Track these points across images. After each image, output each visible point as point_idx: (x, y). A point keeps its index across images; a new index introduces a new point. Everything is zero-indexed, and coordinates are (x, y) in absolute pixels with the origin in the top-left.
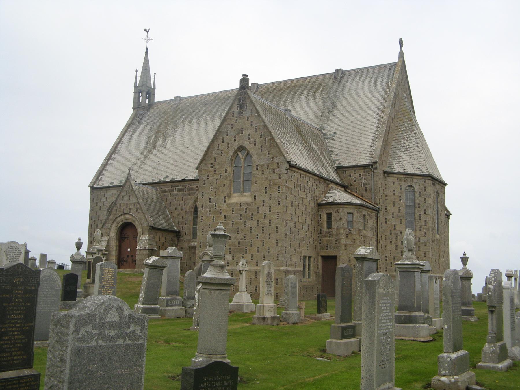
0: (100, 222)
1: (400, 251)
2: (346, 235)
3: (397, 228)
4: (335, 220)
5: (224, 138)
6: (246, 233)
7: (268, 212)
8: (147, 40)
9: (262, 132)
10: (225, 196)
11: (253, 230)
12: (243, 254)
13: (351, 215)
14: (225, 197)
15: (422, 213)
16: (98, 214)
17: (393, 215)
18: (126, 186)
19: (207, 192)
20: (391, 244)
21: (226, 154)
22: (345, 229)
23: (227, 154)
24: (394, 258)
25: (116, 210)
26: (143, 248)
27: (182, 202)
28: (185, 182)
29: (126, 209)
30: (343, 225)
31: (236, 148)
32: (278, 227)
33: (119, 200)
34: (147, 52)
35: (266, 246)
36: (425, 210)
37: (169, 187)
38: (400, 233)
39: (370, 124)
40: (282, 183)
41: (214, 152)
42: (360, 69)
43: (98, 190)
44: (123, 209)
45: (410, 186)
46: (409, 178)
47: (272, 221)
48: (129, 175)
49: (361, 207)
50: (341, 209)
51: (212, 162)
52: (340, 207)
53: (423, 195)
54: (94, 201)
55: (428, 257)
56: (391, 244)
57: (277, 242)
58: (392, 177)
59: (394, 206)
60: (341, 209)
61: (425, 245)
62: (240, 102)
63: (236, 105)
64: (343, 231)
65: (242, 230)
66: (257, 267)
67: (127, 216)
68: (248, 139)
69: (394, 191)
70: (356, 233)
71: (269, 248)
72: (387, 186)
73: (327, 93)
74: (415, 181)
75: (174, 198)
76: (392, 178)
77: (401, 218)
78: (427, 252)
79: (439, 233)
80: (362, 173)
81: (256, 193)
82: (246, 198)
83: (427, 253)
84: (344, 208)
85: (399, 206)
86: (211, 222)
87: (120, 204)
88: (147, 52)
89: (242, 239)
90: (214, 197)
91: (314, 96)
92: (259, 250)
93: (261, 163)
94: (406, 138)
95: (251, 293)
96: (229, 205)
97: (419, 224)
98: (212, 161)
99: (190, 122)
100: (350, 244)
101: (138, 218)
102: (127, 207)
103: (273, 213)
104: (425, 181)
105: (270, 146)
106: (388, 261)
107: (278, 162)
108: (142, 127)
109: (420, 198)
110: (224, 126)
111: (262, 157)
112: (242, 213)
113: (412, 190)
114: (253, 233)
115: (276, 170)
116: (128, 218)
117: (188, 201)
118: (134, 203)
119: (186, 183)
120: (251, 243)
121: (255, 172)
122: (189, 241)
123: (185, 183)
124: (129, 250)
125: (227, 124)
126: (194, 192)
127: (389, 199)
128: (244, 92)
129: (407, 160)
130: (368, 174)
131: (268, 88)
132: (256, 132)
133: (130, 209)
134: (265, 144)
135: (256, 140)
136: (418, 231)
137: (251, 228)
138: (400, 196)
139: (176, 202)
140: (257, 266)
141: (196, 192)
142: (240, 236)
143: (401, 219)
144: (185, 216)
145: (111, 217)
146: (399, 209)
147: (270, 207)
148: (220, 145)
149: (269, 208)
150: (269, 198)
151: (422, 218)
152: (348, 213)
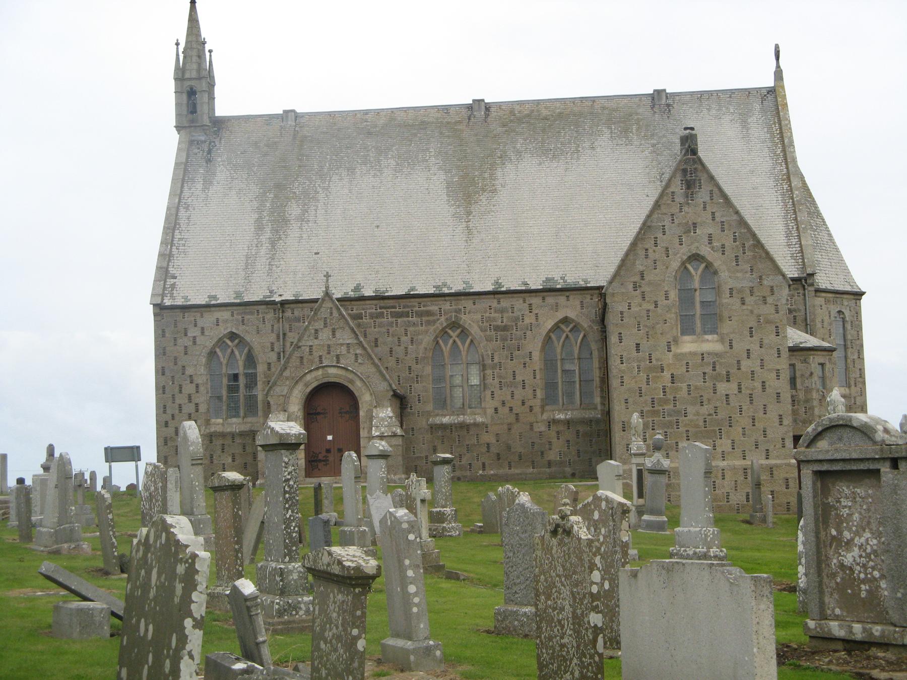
0: (188, 379)
4: (802, 375)
5: (657, 238)
6: (718, 404)
7: (759, 368)
9: (735, 233)
10: (670, 340)
11: (730, 399)
12: (714, 440)
14: (669, 342)
16: (180, 363)
18: (322, 310)
19: (629, 333)
21: (664, 267)
23: (667, 268)
25: (302, 358)
26: (390, 434)
27: (404, 339)
28: (412, 300)
29: (328, 356)
31: (685, 257)
32: (779, 394)
33: (306, 338)
35: (760, 425)
37: (371, 308)
39: (768, 202)
40: (781, 321)
41: (637, 262)
42: (702, 93)
43: (178, 310)
44: (320, 357)
47: (767, 384)
48: (327, 288)
50: (811, 357)
51: (635, 280)
52: (810, 355)
54: (167, 335)
57: (780, 419)
60: (811, 357)
62: (685, 175)
63: (678, 181)
65: (709, 400)
66: (745, 461)
67: (332, 371)
68: (709, 243)
71: (765, 428)
73: (653, 135)
75: (384, 330)
76: (819, 299)
81: (731, 336)
82: (711, 344)
84: (815, 356)
86: (644, 387)
87: (311, 346)
89: (710, 415)
90: (645, 342)
91: (627, 138)
92: (747, 433)
93: (739, 286)
95: (738, 504)
96: (678, 357)
98: (637, 278)
99: (351, 170)
101: (361, 374)
102: (329, 353)
103: (768, 370)
105: (754, 257)
107: (771, 284)
108: (222, 174)
110: (655, 216)
111: (739, 275)
112: (706, 371)
114: (732, 405)
115: (768, 299)
116: (334, 374)
117: (420, 337)
118: (348, 344)
119: (414, 302)
121: (726, 301)
122: (429, 414)
123: (410, 302)
124: (330, 438)
125: (662, 214)
126: (435, 318)
128: (693, 160)
130: (798, 293)
131: (512, 112)
132: (724, 231)
133: (338, 357)
134: (744, 253)
135: (724, 245)
136: (853, 387)
137: (727, 395)
139: (390, 339)
140: (744, 459)
141: (438, 320)
142: (705, 409)
144: (414, 367)
145: (287, 373)
147: (762, 360)
148: (650, 251)
149: (759, 361)
150: (759, 345)
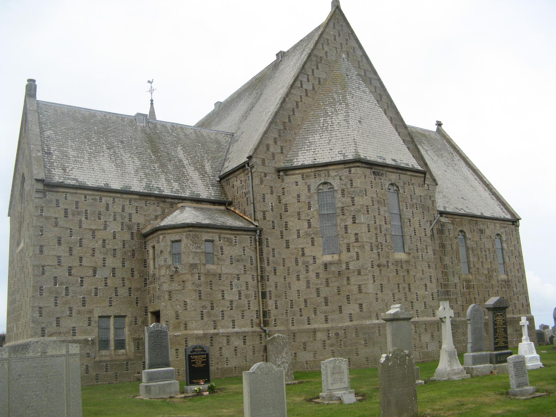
1: (315, 290)
2: (171, 276)
3: (307, 252)
8: (151, 91)
13: (211, 243)
15: (349, 222)
17: (299, 233)
20: (298, 279)
22: (169, 267)
24: (305, 301)
30: (165, 261)
34: (152, 104)
36: (354, 217)
38: (312, 260)
45: (325, 183)
46: (322, 170)
49: (191, 229)
50: (161, 237)
53: (349, 193)
55: (366, 293)
56: (298, 279)
58: (293, 175)
59: (299, 219)
60: (161, 237)
61: (359, 274)
64: (166, 270)
69: (299, 196)
70: (186, 271)
72: (286, 190)
74: (333, 173)
77: (313, 236)
78: (364, 284)
79: (406, 250)
80: (243, 179)
83: (363, 287)
85: (309, 218)
88: (152, 104)
94: (330, 114)
97: (346, 241)
100: (177, 290)
104: (350, 171)
106: (296, 309)
109: (343, 200)
113: (330, 188)
120: (299, 295)
127: (290, 209)
129: (323, 144)
138: (309, 202)
143: (312, 238)
146: (308, 223)
151: (349, 231)
152: (173, 242)
